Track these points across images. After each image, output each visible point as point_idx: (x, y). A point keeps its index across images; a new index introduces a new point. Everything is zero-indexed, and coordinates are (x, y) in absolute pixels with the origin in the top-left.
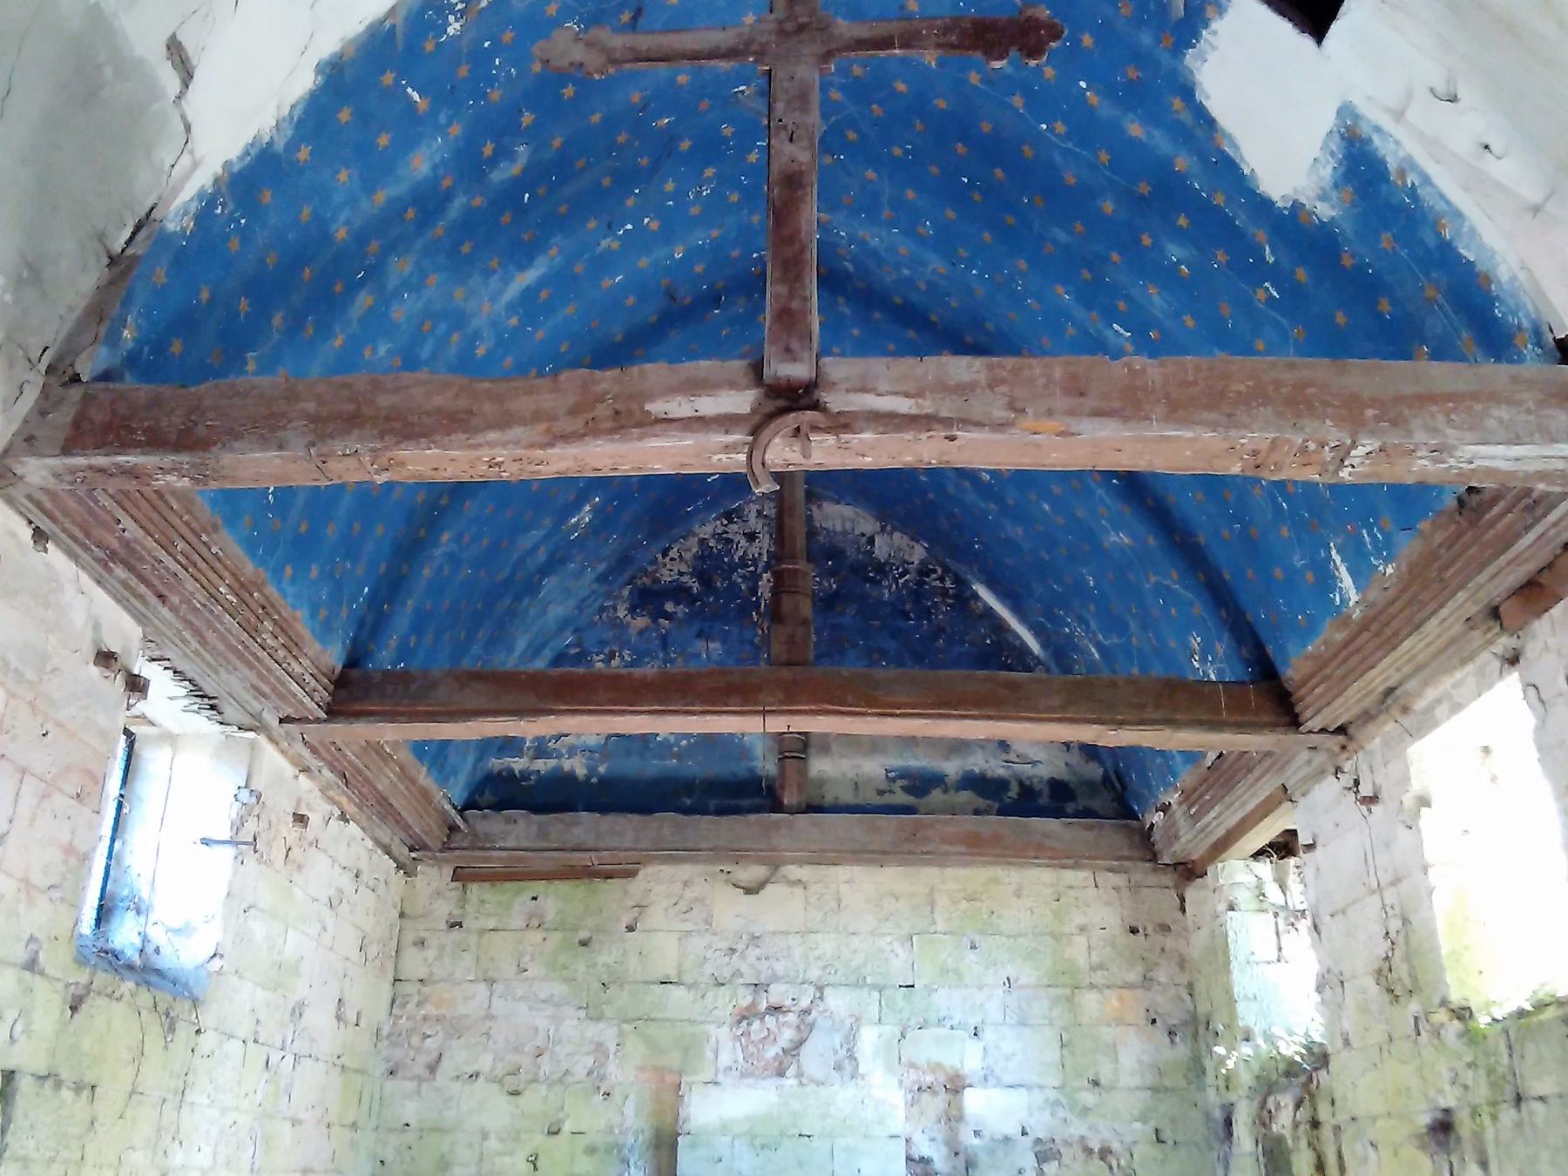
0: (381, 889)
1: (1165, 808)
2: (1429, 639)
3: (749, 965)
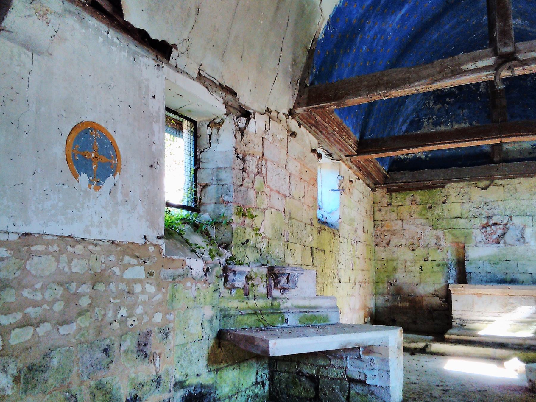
3: (485, 211)
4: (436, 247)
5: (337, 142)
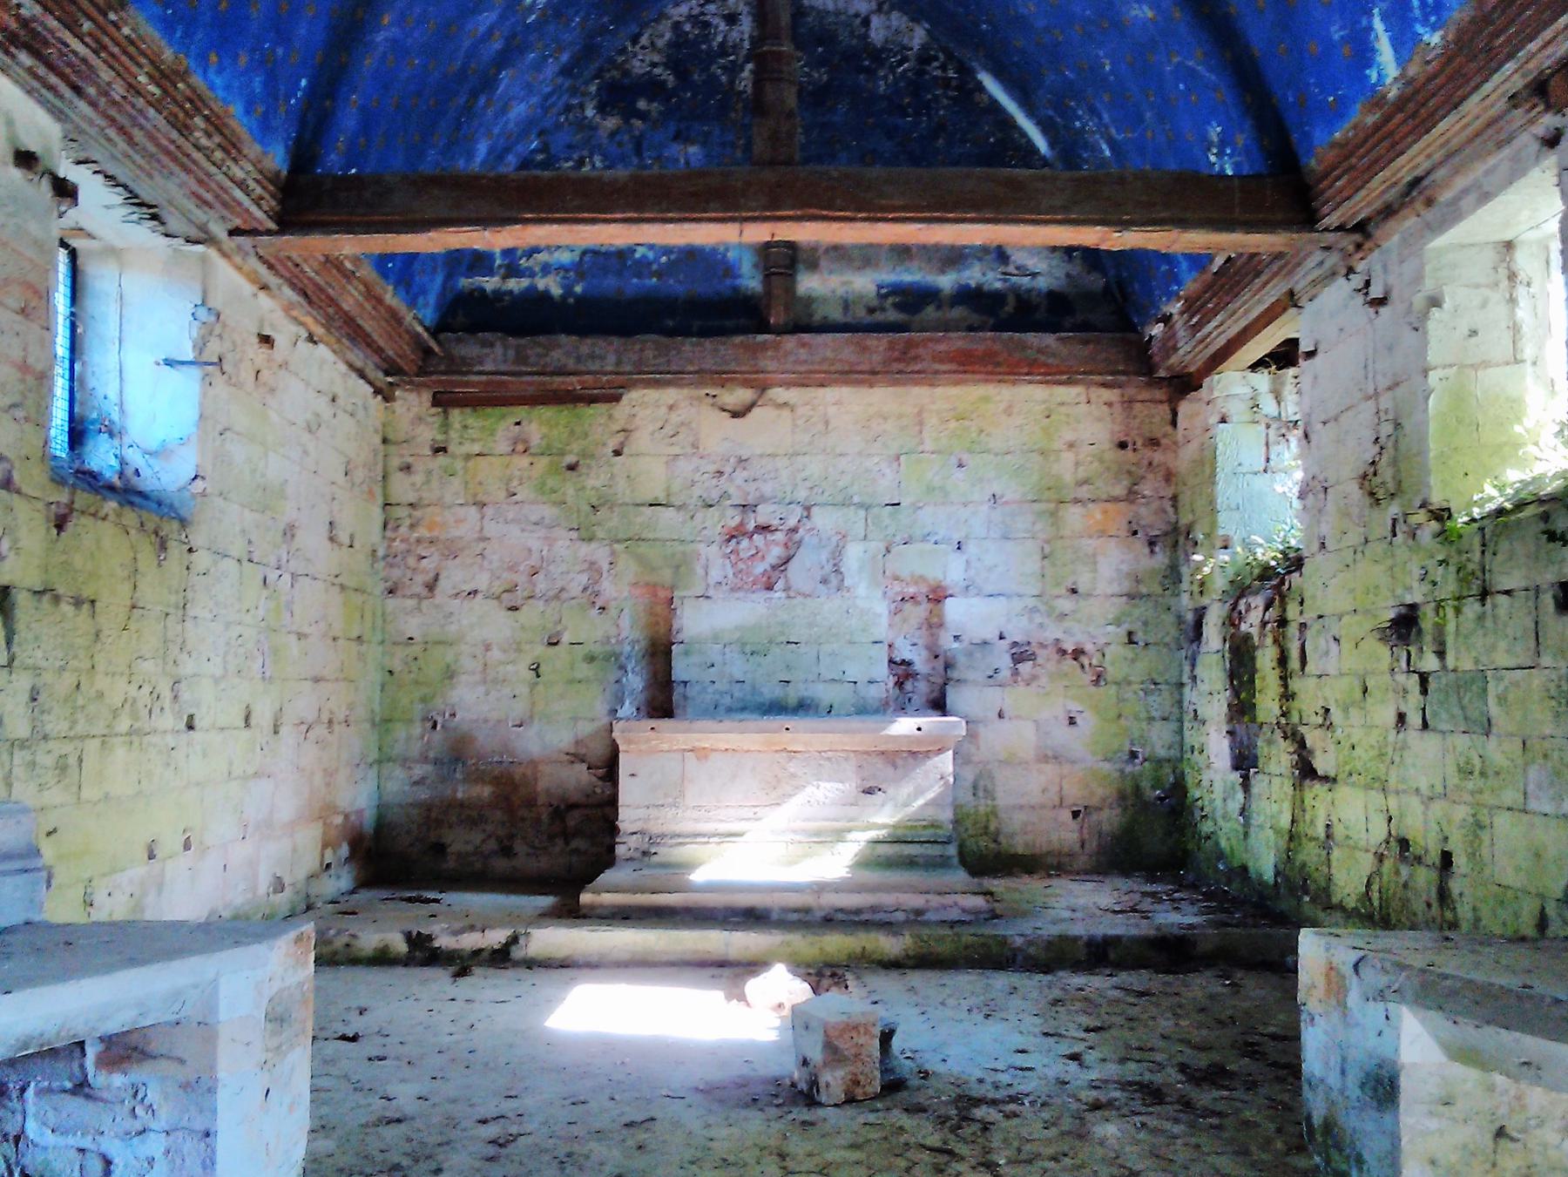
0: (361, 414)
1: (1167, 319)
2: (1465, 121)
3: (737, 487)
4: (584, 600)
5: (168, 153)
